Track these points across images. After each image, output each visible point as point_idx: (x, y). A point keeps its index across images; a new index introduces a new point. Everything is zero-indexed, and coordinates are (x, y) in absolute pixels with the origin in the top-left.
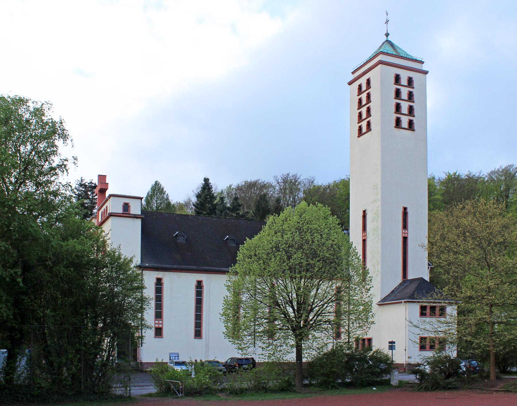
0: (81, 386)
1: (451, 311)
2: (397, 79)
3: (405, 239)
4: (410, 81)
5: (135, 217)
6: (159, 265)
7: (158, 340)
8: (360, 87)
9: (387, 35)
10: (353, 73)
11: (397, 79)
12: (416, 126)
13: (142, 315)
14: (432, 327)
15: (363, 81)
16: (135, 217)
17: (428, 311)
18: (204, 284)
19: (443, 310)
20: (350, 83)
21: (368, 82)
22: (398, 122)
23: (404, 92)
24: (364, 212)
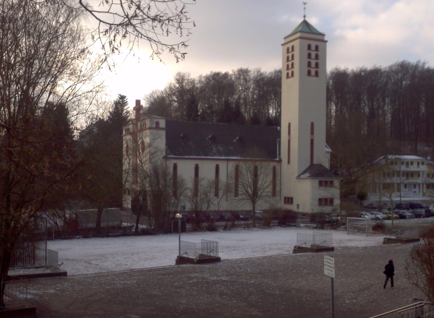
0: (197, 273)
1: (337, 183)
2: (309, 47)
3: (312, 141)
4: (317, 48)
5: (162, 129)
6: (175, 156)
7: (312, 121)
8: (288, 49)
9: (305, 16)
10: (285, 38)
11: (309, 47)
12: (320, 74)
13: (178, 202)
14: (325, 193)
15: (290, 45)
16: (162, 129)
17: (323, 183)
18: (200, 166)
19: (332, 182)
20: (283, 45)
21: (293, 47)
22: (309, 73)
23: (313, 54)
24: (312, 125)
